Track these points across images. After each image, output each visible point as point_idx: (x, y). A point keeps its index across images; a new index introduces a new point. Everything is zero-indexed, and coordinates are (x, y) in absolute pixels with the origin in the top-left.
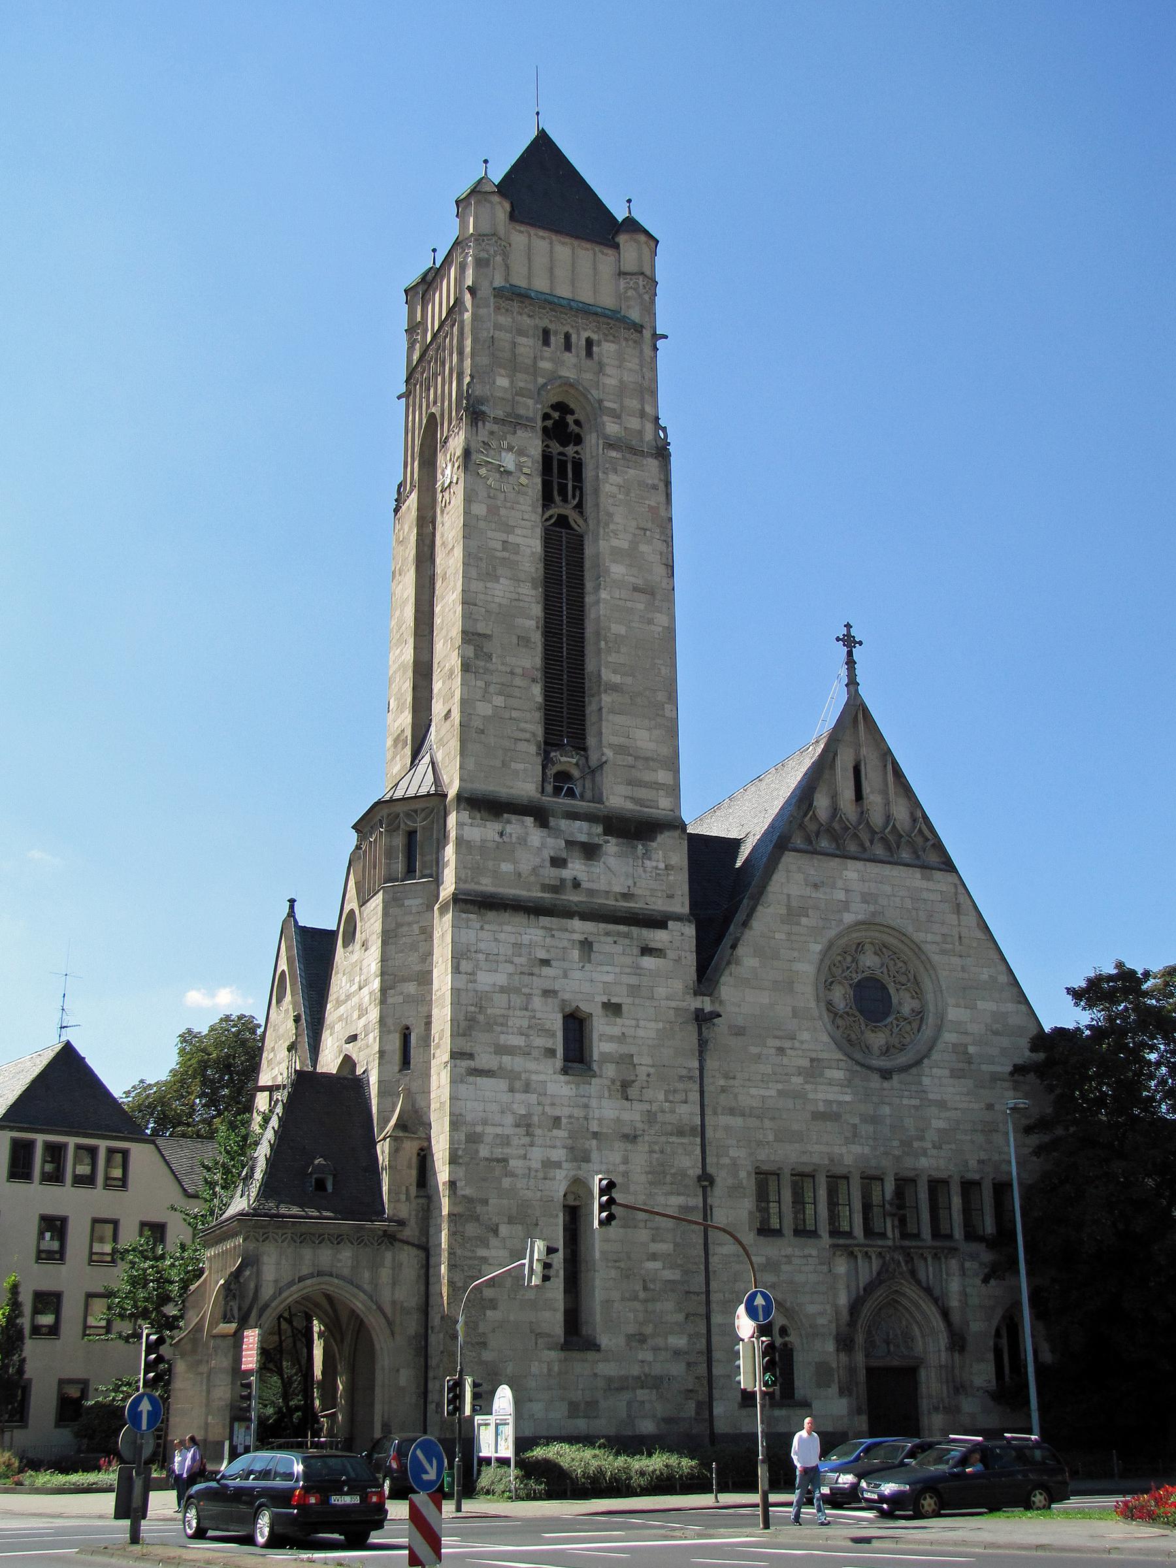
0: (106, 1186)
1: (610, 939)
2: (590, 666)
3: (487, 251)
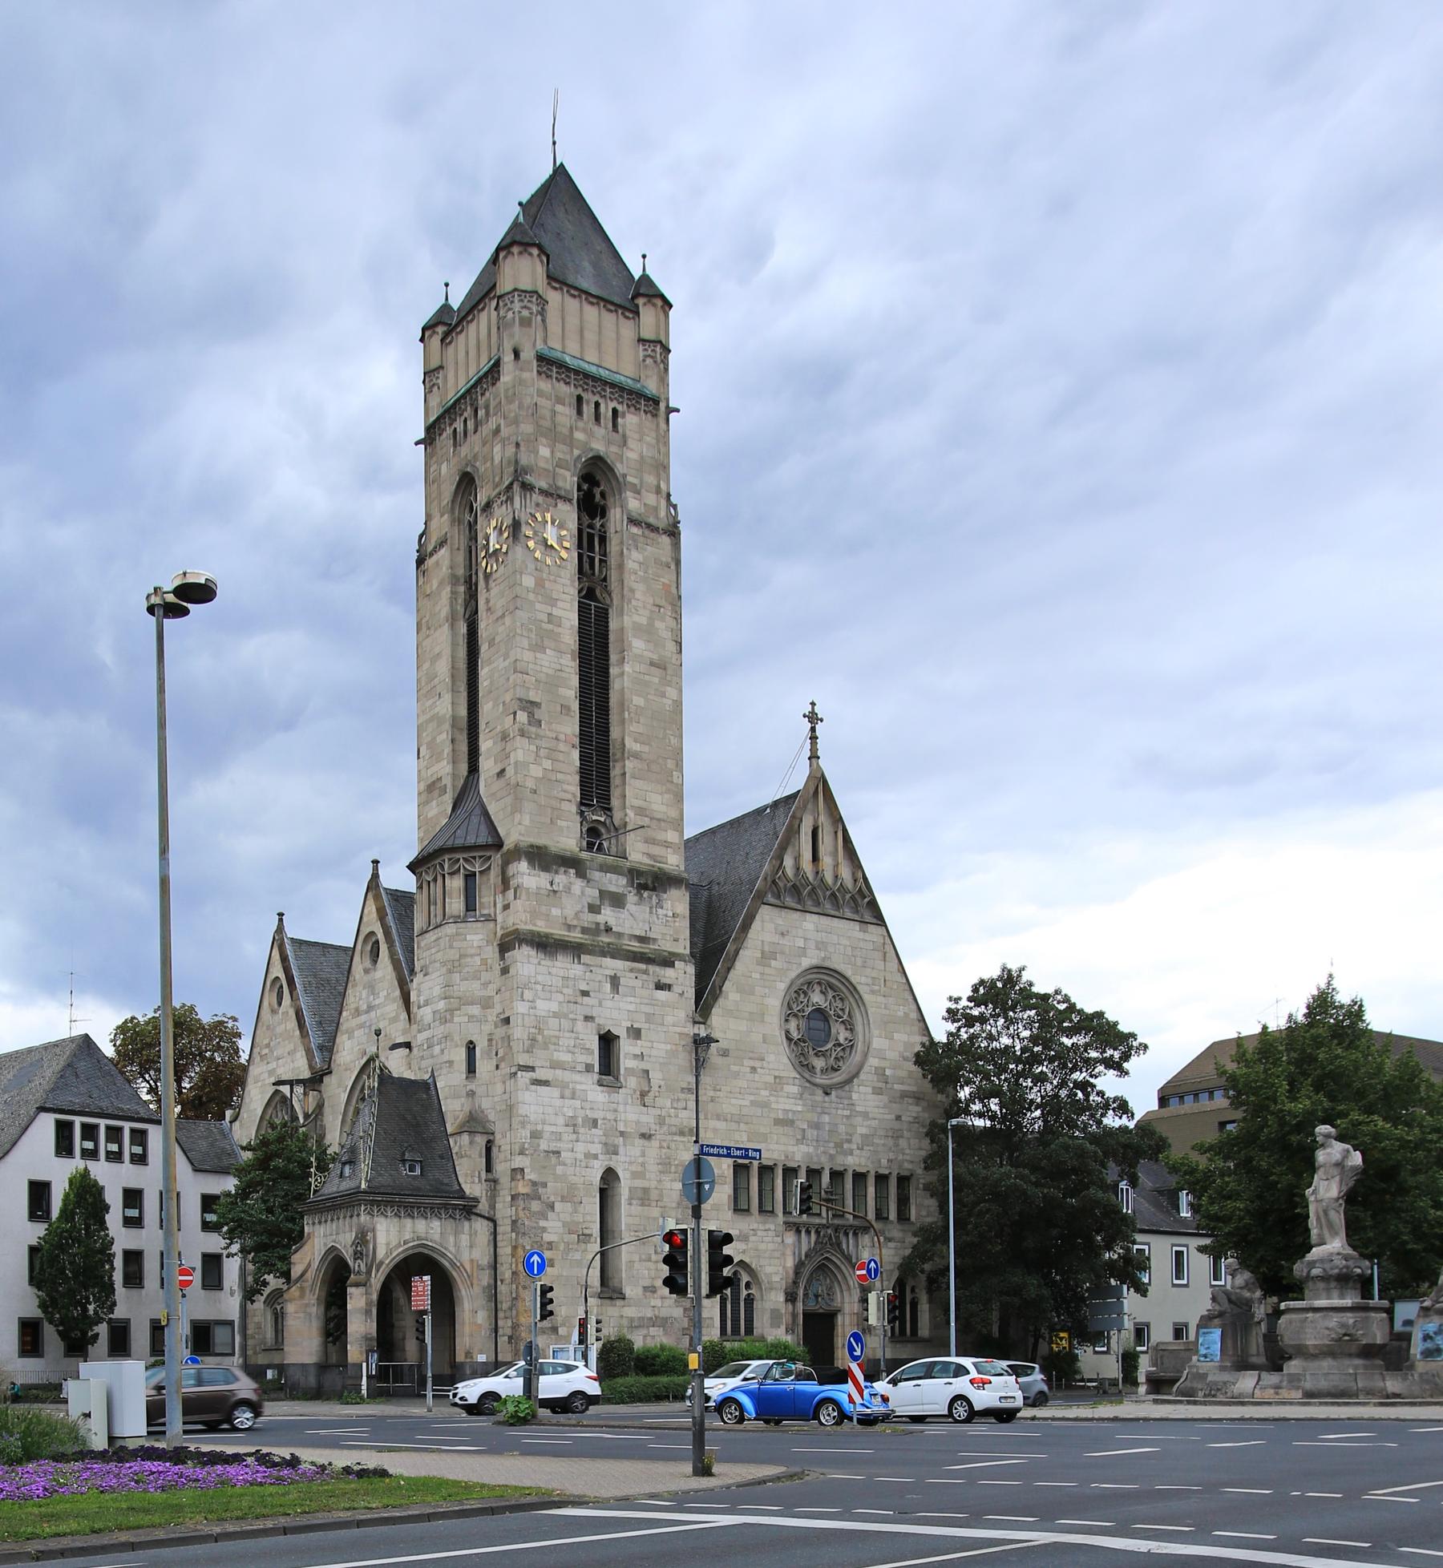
0: (108, 1159)
1: (633, 975)
2: (615, 733)
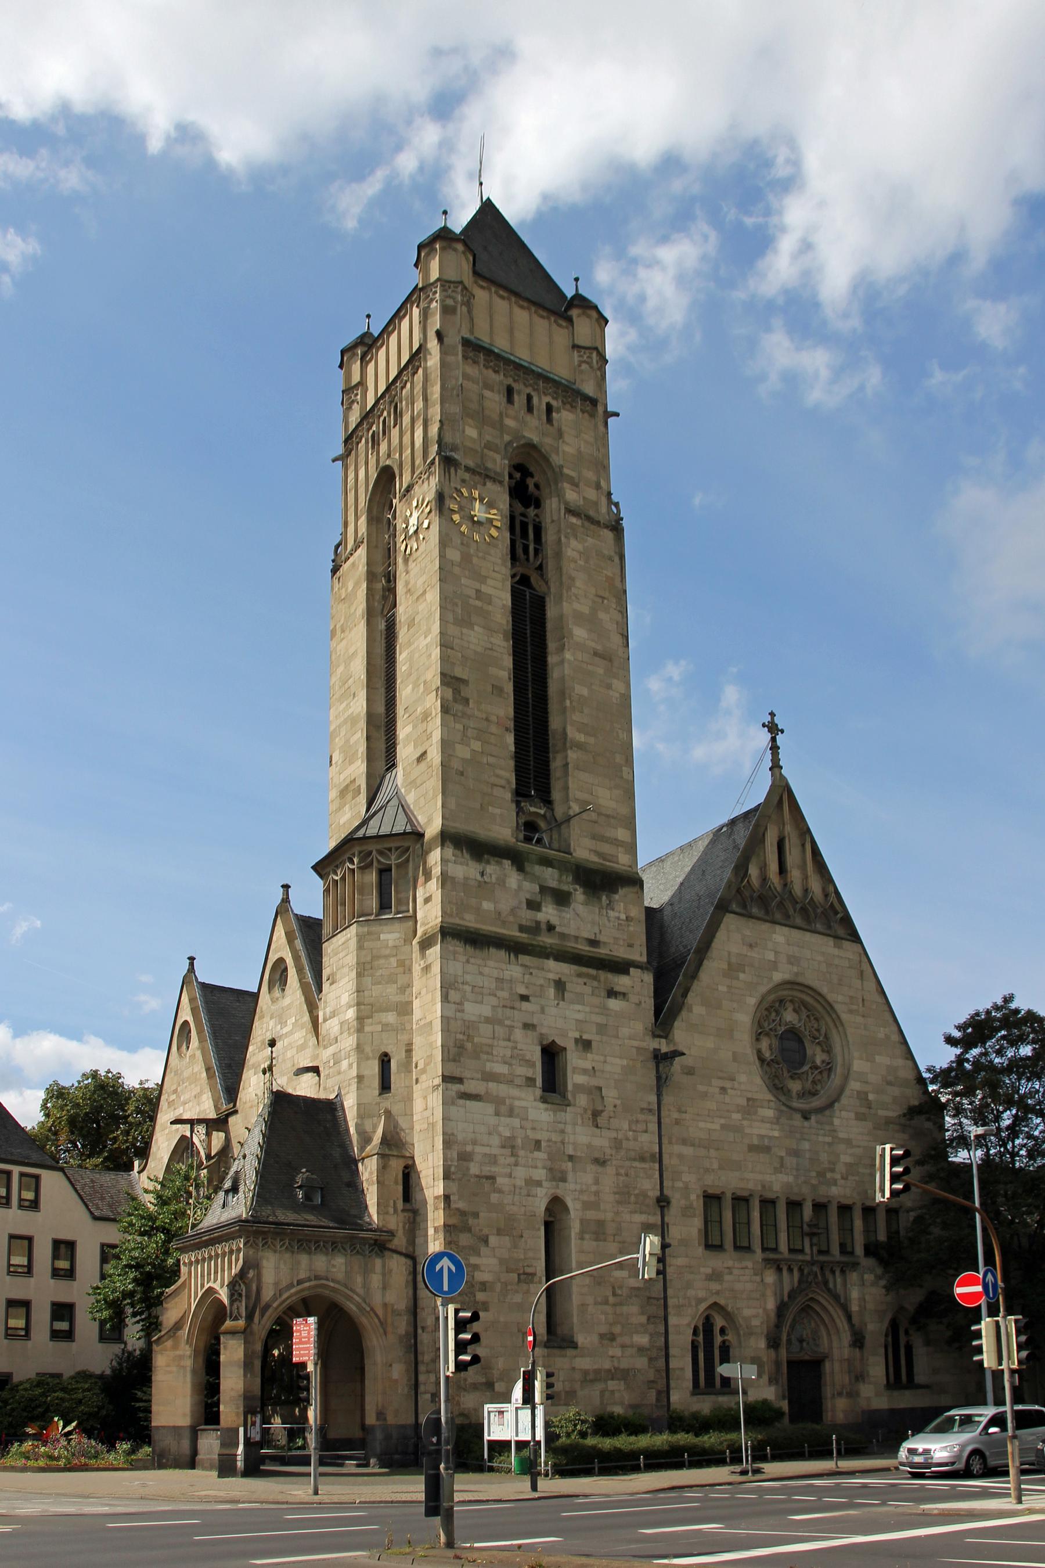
0: (21, 1207)
1: (581, 981)
2: (555, 723)
3: (454, 299)
